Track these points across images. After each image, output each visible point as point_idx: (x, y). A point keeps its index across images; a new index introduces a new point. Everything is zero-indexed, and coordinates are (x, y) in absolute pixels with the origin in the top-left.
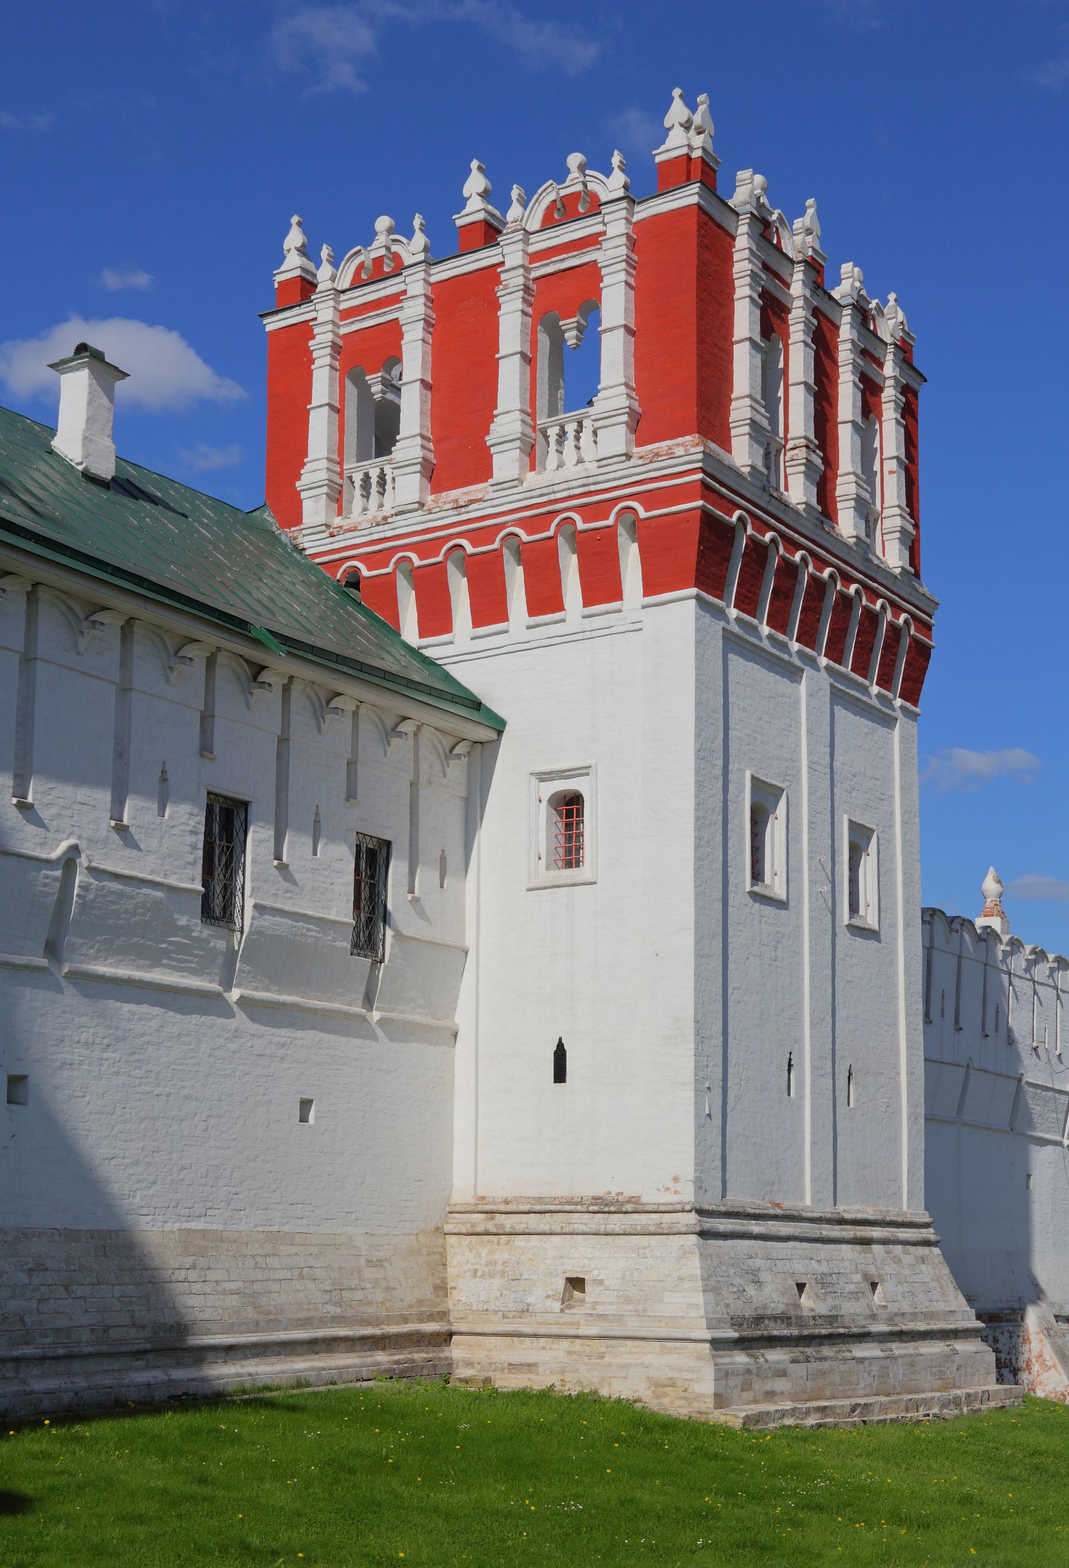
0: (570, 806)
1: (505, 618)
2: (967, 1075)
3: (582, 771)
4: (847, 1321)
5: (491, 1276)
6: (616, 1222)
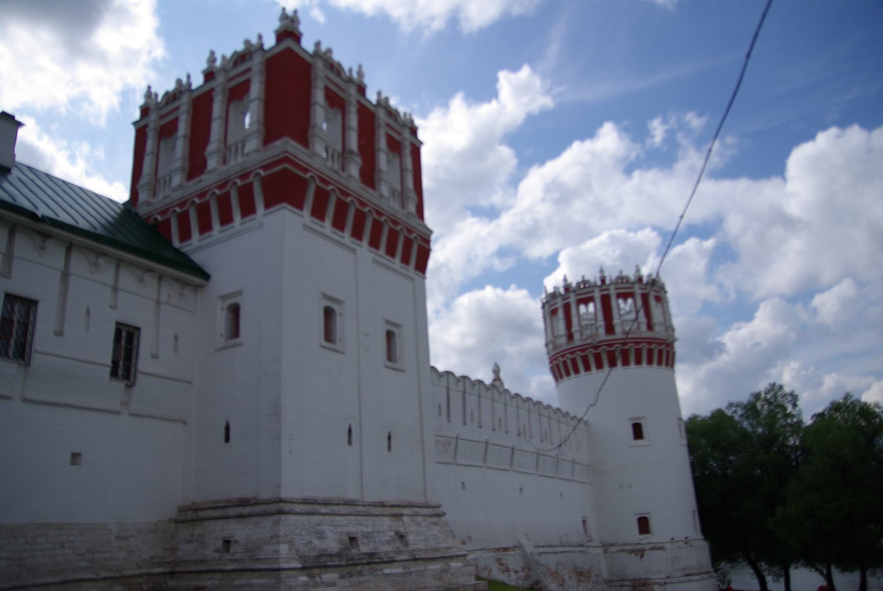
0: (235, 311)
2: (486, 446)
3: (239, 293)
4: (382, 555)
6: (247, 510)
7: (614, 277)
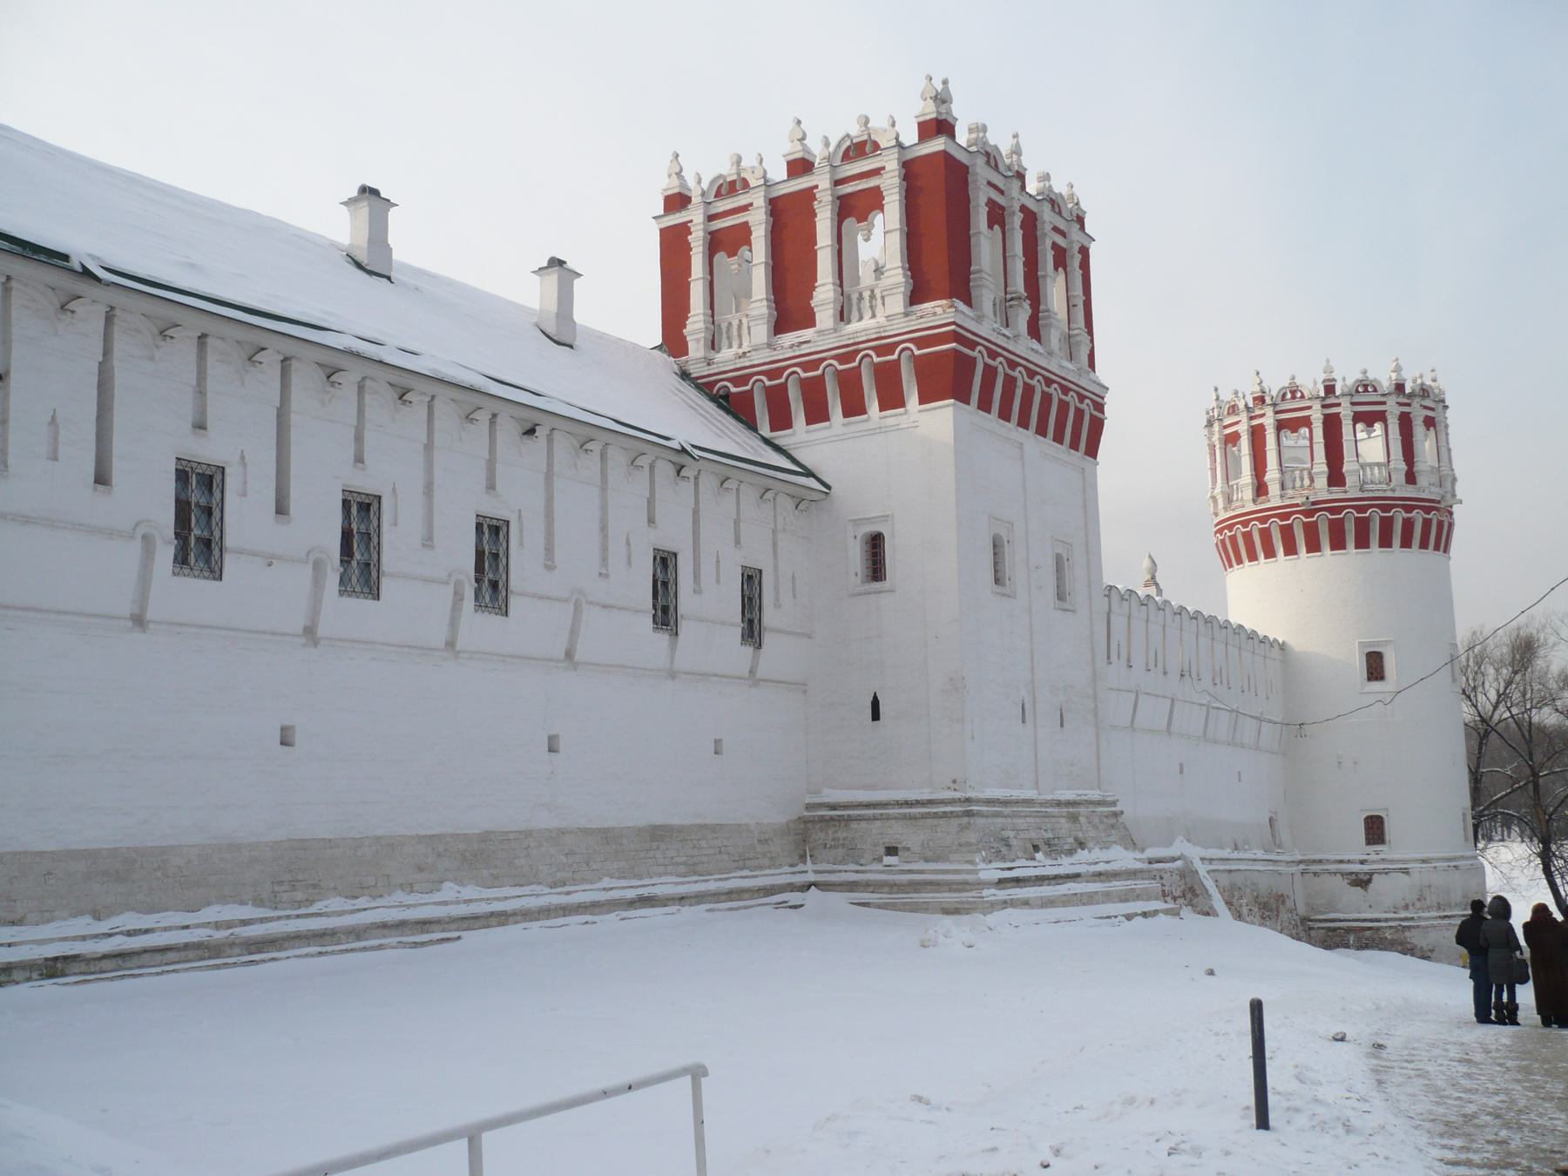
1: (828, 419)
3: (884, 518)
5: (836, 847)
7: (1350, 381)
